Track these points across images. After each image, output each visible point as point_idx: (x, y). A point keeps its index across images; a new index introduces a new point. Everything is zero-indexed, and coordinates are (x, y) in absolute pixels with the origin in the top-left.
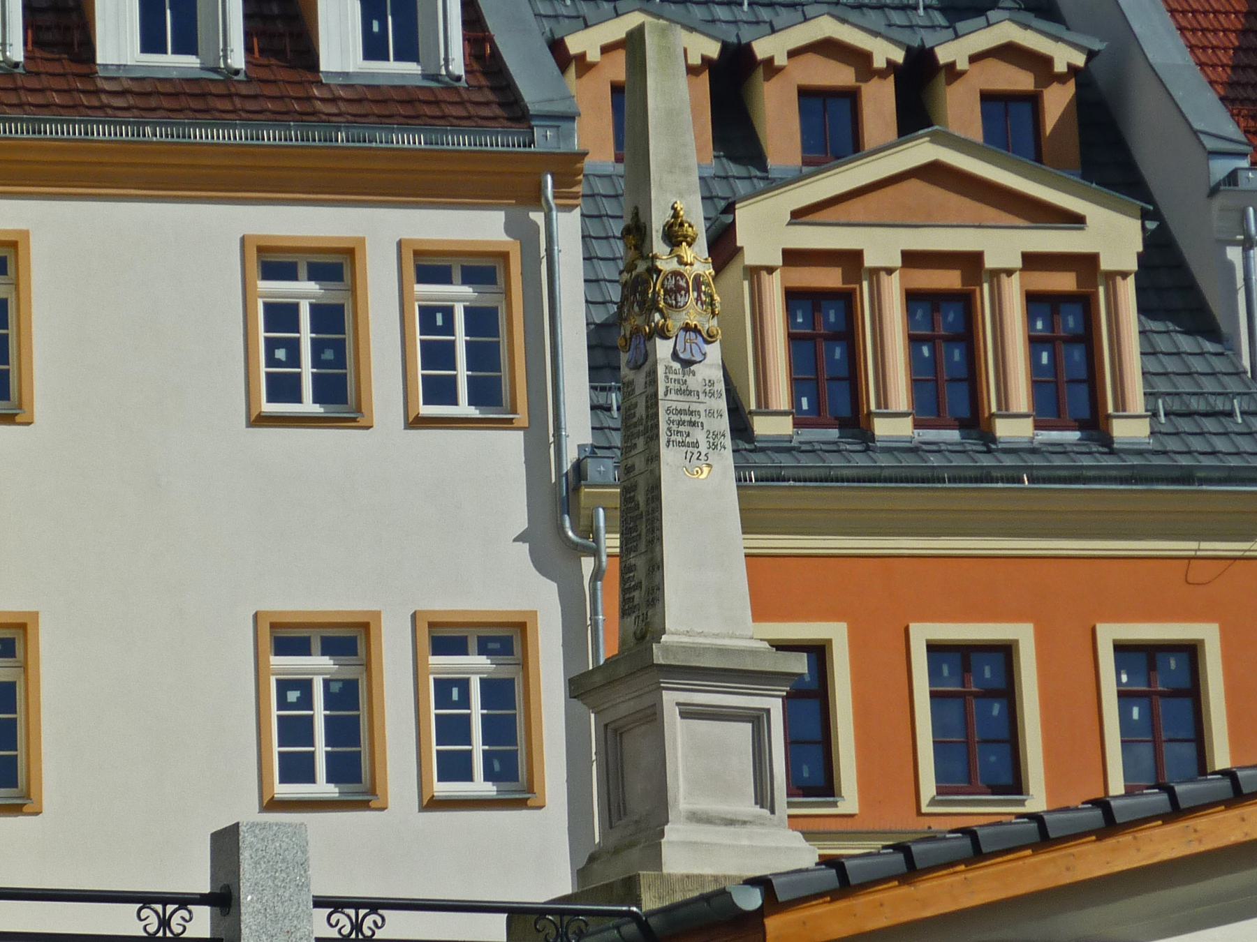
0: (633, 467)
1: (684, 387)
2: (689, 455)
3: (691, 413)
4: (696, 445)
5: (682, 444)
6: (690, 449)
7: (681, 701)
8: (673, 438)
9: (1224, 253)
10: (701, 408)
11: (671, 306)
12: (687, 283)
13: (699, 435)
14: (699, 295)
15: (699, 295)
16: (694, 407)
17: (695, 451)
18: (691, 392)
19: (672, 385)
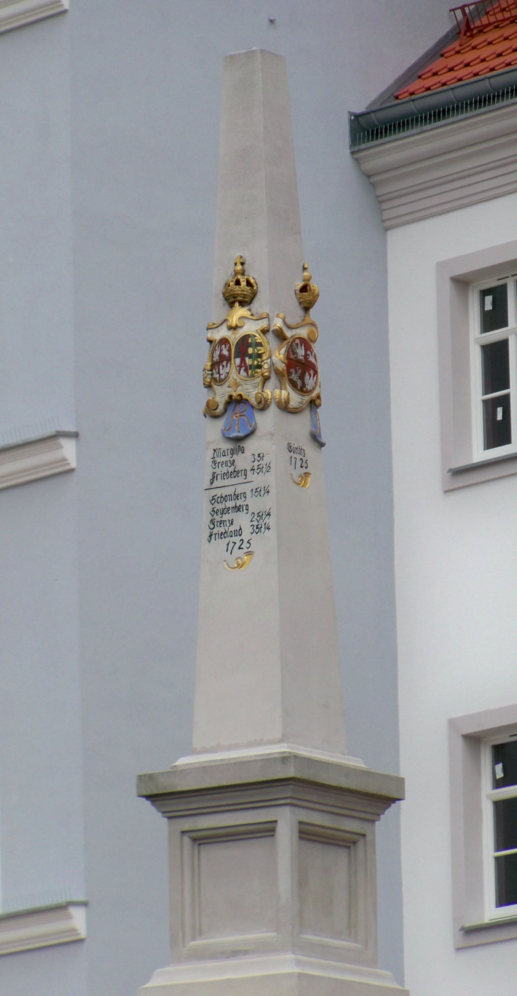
0: (300, 476)
1: (231, 469)
2: (231, 545)
3: (237, 497)
4: (239, 533)
5: (222, 535)
6: (234, 539)
7: (186, 828)
8: (215, 531)
9: (499, 421)
10: (246, 488)
11: (215, 379)
12: (229, 350)
13: (243, 521)
14: (243, 360)
15: (243, 360)
16: (240, 489)
17: (237, 539)
18: (238, 472)
19: (218, 471)
